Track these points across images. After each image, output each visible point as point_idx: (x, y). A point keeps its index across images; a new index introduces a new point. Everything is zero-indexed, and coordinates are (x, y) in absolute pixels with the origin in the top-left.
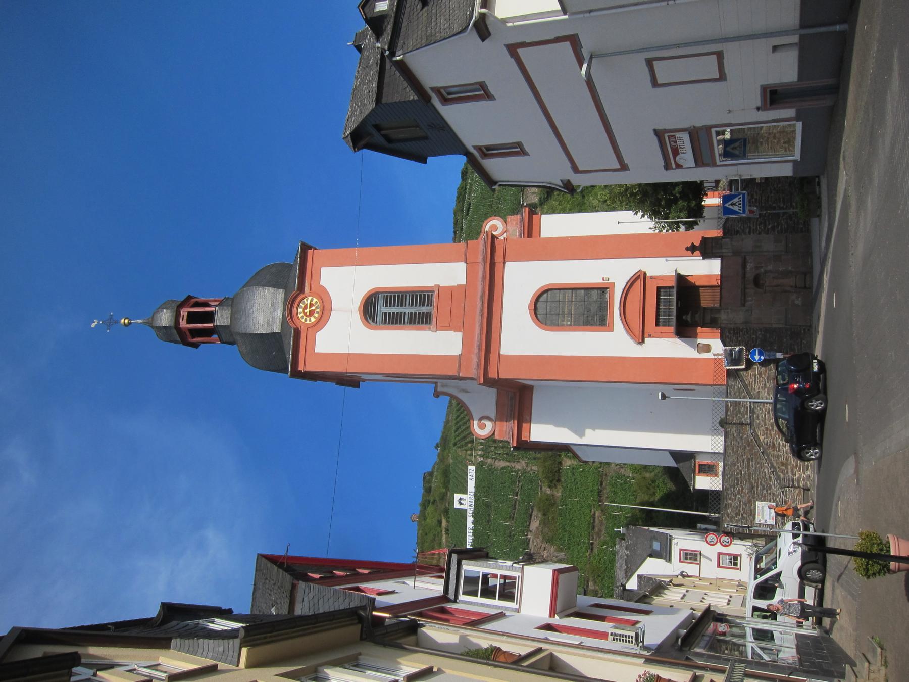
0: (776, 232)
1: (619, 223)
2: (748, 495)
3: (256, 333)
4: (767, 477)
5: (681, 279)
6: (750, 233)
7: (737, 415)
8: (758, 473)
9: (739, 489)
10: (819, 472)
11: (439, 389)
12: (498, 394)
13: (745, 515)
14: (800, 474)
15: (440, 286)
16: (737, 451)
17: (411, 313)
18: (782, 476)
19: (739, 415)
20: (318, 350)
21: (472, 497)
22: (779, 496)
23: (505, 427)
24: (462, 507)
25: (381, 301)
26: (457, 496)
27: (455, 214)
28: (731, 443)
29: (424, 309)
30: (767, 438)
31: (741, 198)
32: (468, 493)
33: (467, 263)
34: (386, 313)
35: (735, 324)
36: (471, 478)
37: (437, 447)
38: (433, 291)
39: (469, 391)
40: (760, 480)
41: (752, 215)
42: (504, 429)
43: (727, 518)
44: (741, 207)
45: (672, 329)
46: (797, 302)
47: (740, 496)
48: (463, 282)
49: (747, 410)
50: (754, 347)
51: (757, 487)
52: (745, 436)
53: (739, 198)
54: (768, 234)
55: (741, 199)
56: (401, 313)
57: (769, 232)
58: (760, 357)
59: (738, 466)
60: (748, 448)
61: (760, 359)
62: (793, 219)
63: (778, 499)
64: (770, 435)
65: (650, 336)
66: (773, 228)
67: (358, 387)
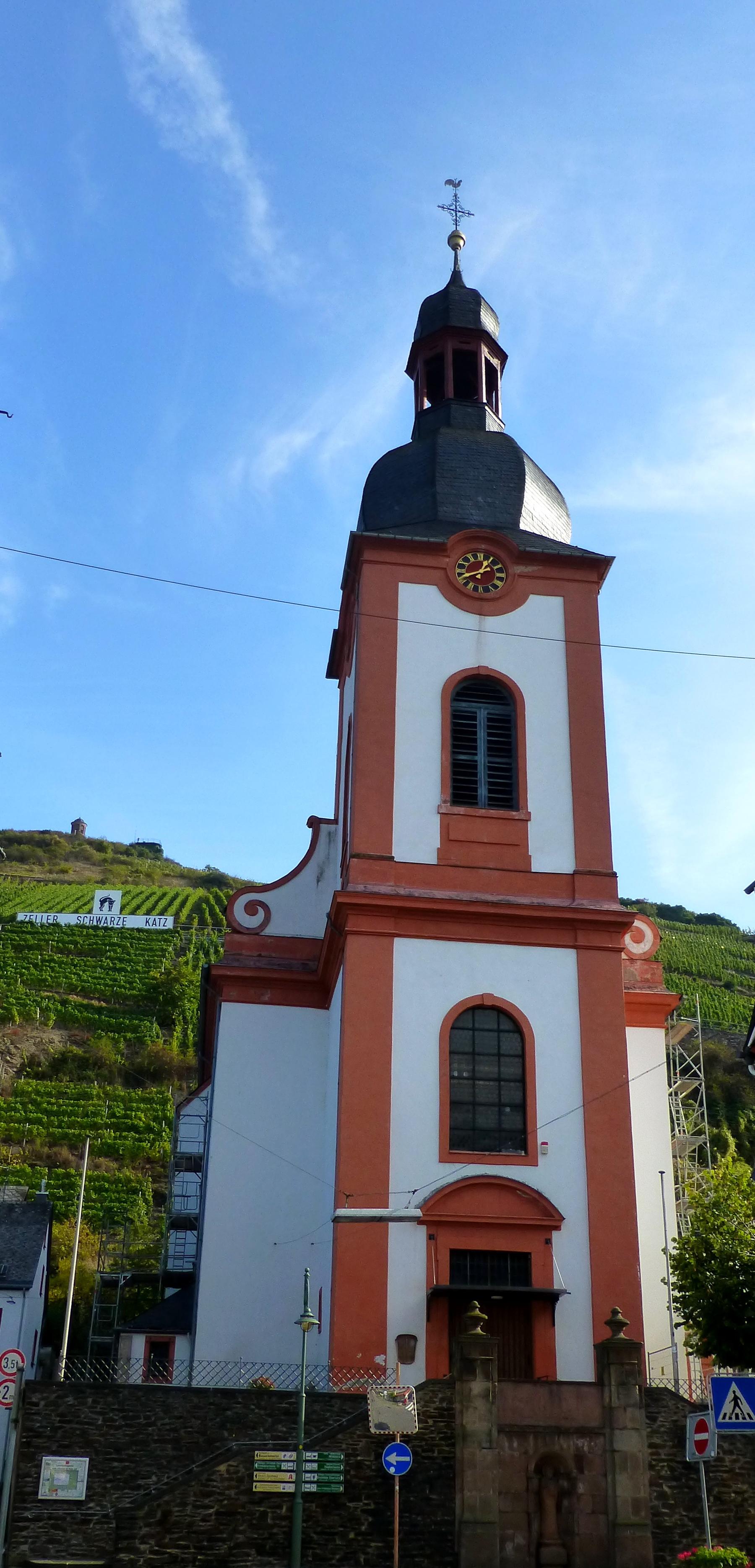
0: (656, 1503)
1: (662, 1173)
2: (102, 1439)
3: (437, 475)
4: (141, 1482)
5: (551, 1298)
6: (651, 1446)
7: (269, 1415)
8: (149, 1462)
9: (116, 1421)
10: (499, 323)
11: (323, 827)
12: (314, 941)
13: (60, 1434)
14: (144, 1552)
15: (529, 823)
16: (194, 1417)
17: (475, 767)
18: (141, 1513)
19: (270, 1420)
20: (405, 589)
21: (115, 922)
22: (98, 1508)
23: (249, 953)
24: (96, 904)
25: (497, 709)
26: (116, 895)
27: (638, 902)
28: (211, 1404)
29: (483, 791)
30: (223, 1480)
31: (751, 1418)
32: (122, 916)
33: (573, 875)
34: (475, 719)
35: (461, 1412)
36: (151, 922)
37: (208, 867)
38: (517, 810)
39: (319, 884)
40: (133, 1465)
41: (690, 1447)
42: (244, 952)
43: (55, 1395)
44: (730, 1418)
45: (445, 1282)
46: (509, 1547)
47: (100, 1422)
48: (537, 866)
49: (279, 1438)
50: (415, 1454)
51: (120, 1460)
52: (226, 1434)
53: (749, 1414)
54: (652, 1484)
55: (748, 1420)
56: (475, 748)
57: (655, 1488)
58: (392, 1465)
59: (163, 1419)
60: (201, 1440)
61: (390, 1465)
62: (684, 1541)
63: (91, 1505)
64: (229, 1488)
65: (431, 1237)
66: (662, 1496)
67: (330, 674)
